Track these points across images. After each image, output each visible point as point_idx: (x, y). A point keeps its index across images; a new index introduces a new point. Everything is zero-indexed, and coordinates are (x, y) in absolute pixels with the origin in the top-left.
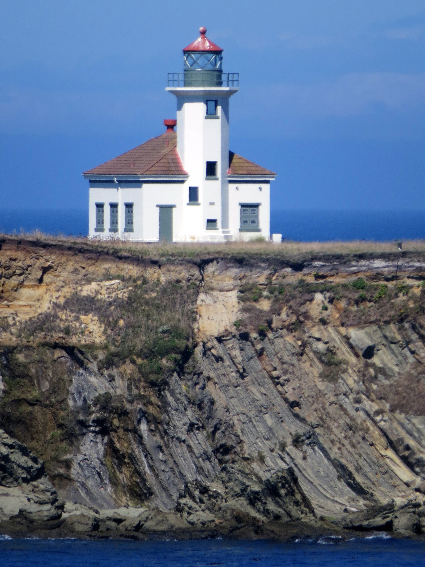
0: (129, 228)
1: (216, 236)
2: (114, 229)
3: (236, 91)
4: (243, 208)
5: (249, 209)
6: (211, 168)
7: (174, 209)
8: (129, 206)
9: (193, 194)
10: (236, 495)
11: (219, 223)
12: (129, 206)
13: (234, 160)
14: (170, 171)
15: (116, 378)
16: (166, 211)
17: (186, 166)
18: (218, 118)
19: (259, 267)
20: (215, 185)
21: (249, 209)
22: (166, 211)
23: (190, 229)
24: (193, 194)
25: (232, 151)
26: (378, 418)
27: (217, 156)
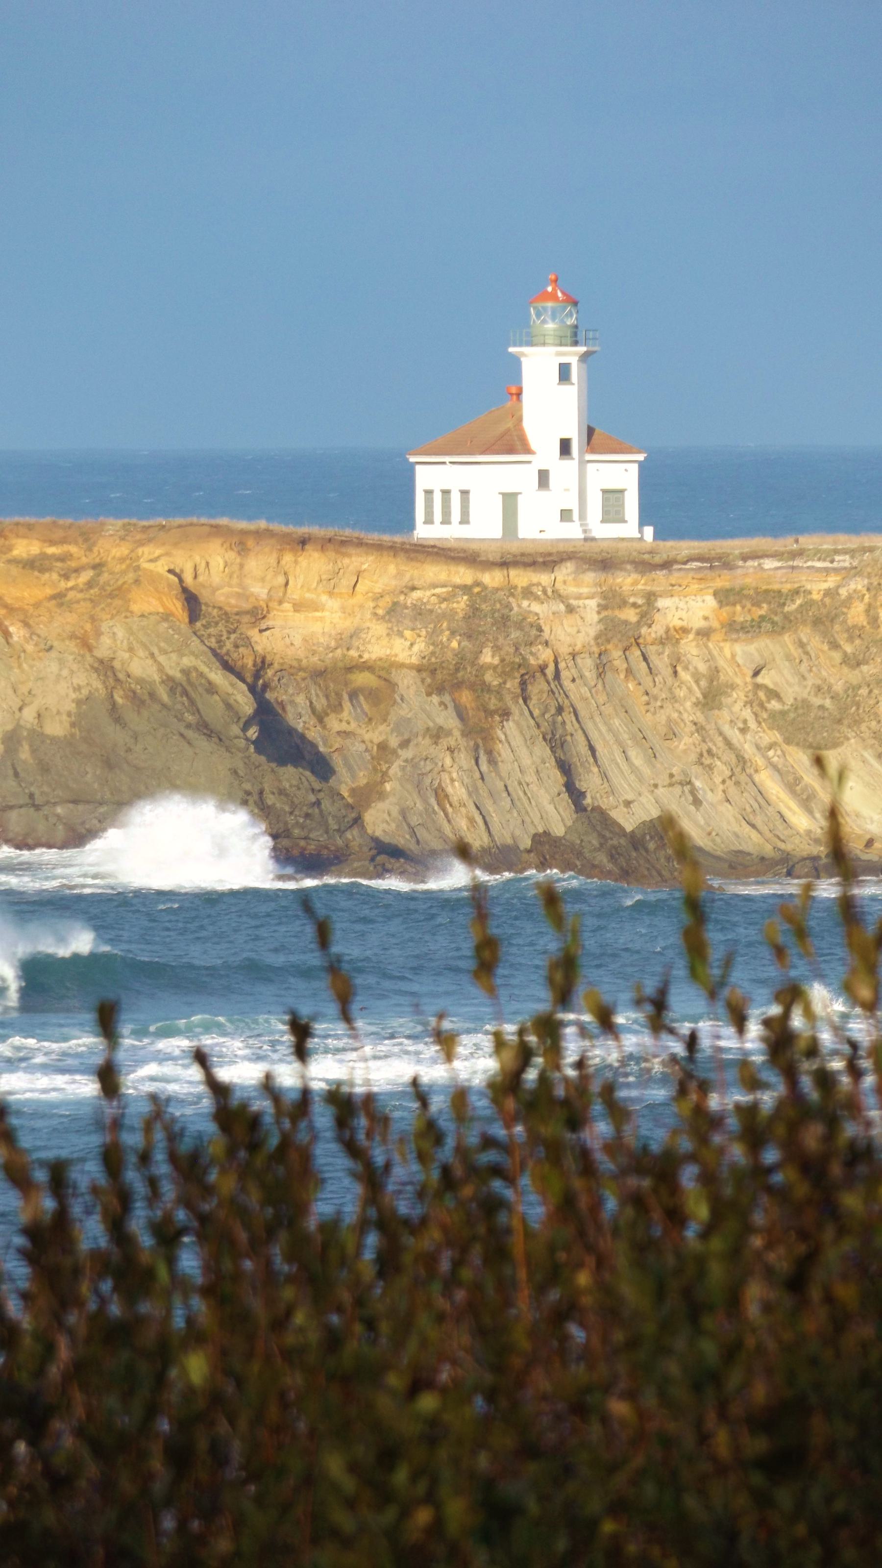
0: (465, 520)
1: (572, 531)
2: (446, 521)
3: (594, 352)
4: (606, 495)
5: (612, 499)
6: (565, 447)
7: (519, 496)
8: (465, 493)
9: (543, 478)
10: (595, 849)
11: (576, 515)
12: (465, 493)
13: (595, 437)
14: (513, 443)
15: (396, 1137)
16: (510, 500)
17: (533, 441)
18: (573, 384)
19: (625, 570)
20: (571, 465)
21: (612, 499)
22: (510, 500)
23: (540, 524)
24: (543, 478)
25: (591, 425)
26: (771, 753)
27: (573, 432)
